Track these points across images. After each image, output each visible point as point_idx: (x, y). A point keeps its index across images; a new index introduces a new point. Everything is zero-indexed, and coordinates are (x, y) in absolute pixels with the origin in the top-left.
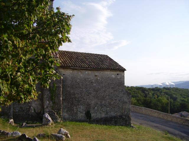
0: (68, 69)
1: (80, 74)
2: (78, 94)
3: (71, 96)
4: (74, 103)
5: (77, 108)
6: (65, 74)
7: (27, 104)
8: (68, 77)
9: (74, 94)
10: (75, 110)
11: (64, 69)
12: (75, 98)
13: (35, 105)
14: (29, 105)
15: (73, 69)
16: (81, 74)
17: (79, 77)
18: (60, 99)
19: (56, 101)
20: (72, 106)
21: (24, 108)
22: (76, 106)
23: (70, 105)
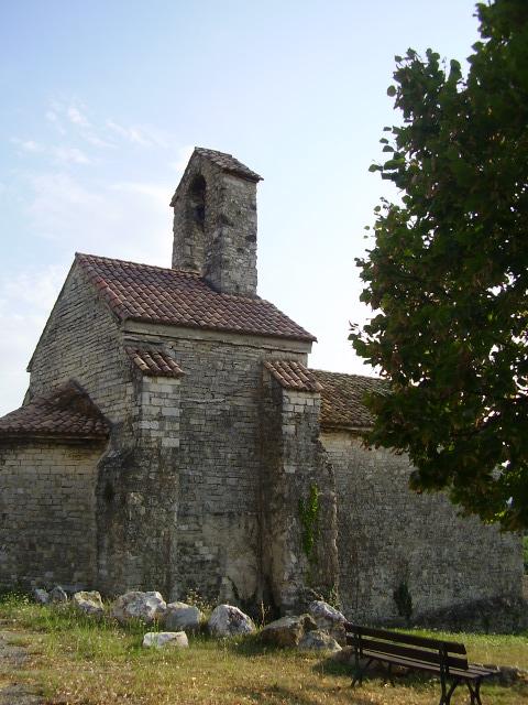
2: (372, 525)
5: (368, 578)
7: (211, 569)
8: (339, 463)
9: (359, 526)
10: (362, 583)
12: (363, 539)
17: (372, 463)
18: (328, 548)
22: (367, 570)
23: (346, 565)
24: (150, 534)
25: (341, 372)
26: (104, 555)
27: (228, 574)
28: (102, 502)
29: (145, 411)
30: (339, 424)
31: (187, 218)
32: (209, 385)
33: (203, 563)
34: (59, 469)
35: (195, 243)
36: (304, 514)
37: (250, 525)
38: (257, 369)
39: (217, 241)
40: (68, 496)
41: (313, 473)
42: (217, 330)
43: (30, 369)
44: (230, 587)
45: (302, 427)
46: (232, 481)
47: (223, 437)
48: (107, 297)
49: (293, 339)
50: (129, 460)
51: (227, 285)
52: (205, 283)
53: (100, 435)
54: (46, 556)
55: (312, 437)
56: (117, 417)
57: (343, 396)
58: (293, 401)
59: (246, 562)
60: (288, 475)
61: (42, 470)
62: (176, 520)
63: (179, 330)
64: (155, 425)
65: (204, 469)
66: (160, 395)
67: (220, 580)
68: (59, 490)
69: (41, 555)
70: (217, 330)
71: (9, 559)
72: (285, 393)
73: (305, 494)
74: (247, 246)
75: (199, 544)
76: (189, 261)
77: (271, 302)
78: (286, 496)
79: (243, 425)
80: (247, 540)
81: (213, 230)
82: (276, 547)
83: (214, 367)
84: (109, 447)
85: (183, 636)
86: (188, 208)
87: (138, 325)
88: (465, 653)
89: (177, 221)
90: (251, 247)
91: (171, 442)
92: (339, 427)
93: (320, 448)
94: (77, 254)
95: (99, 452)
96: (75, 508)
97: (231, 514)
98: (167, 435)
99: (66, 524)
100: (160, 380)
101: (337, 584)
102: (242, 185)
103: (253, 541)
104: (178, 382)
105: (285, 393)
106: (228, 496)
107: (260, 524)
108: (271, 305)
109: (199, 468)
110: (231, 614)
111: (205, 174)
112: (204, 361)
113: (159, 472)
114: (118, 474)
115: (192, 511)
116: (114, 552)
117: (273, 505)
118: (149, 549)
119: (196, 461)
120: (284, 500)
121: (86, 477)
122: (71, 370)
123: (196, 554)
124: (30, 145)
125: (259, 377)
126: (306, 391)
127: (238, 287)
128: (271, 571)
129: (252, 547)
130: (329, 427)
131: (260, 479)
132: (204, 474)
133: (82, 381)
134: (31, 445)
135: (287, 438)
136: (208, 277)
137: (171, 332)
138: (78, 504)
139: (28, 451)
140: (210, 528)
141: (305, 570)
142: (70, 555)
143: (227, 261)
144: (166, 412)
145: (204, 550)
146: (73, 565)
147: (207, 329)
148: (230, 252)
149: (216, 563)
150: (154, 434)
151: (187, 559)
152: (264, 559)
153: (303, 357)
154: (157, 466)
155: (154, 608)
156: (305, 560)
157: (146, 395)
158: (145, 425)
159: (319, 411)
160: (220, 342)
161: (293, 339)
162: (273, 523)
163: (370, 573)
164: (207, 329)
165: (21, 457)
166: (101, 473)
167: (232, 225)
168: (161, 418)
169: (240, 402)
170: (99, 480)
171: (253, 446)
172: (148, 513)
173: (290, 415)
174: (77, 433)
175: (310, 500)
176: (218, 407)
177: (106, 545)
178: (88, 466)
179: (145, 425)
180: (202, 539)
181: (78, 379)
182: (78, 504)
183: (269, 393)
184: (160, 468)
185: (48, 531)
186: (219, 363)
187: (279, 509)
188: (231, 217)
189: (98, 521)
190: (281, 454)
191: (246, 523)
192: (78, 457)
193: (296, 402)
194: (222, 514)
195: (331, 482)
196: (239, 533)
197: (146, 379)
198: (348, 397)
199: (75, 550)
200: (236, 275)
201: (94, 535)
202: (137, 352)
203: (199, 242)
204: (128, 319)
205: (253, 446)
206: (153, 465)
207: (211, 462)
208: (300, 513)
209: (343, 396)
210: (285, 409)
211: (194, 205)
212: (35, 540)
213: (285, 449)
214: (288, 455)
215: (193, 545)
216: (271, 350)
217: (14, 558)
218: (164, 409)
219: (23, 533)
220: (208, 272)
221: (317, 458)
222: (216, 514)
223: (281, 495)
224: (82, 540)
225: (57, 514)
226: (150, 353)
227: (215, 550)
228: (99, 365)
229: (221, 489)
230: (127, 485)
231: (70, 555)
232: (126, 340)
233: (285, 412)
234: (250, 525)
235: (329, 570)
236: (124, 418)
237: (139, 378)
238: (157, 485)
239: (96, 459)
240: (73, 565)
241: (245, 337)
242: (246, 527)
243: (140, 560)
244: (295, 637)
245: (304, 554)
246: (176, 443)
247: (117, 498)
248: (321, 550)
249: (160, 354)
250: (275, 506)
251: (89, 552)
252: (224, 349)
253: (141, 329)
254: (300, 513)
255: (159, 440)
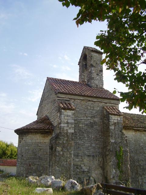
0: (130, 130)
1: (143, 136)
2: (143, 161)
3: (135, 163)
4: (139, 172)
5: (142, 179)
6: (127, 136)
7: (86, 174)
8: (131, 140)
9: (138, 161)
10: (140, 180)
11: (126, 130)
12: (140, 166)
13: (95, 176)
14: (89, 174)
15: (136, 130)
16: (145, 136)
17: (142, 140)
18: (127, 167)
19: (123, 169)
20: (137, 176)
21: (82, 179)
22: (141, 176)
23: (134, 174)
24: (64, 160)
25: (133, 113)
26: (50, 168)
27: (92, 176)
28: (51, 151)
29: (62, 121)
30: (130, 127)
31: (83, 67)
32: (85, 114)
33: (84, 172)
34: (38, 141)
35: (85, 75)
36: (118, 156)
37: (100, 160)
38: (101, 109)
39: (90, 72)
40: (41, 149)
41: (120, 142)
42: (88, 96)
43: (37, 114)
44: (93, 180)
45: (117, 127)
46: (94, 145)
47: (90, 131)
48: (54, 88)
49: (113, 99)
50: (57, 137)
51: (93, 85)
52: (87, 85)
53: (50, 130)
54: (34, 168)
55: (120, 130)
56: (55, 124)
57: (133, 119)
58: (113, 118)
59: (99, 172)
60: (112, 143)
61: (34, 141)
62: (73, 156)
63: (75, 96)
64: (66, 125)
65: (84, 141)
66: (67, 116)
67: (90, 178)
68: (38, 147)
69: (32, 168)
70: (88, 96)
71: (23, 169)
72: (110, 116)
73: (118, 149)
74: (100, 73)
75: (82, 165)
76: (83, 80)
77: (104, 84)
78: (111, 150)
79: (97, 127)
80: (99, 165)
81: (89, 69)
82: (108, 167)
83: (87, 108)
84: (53, 134)
85: (51, 190)
86: (83, 65)
87: (62, 95)
88: (109, 183)
89: (80, 69)
90: (101, 73)
91: (71, 131)
92: (130, 128)
93: (123, 134)
94: (47, 78)
95: (51, 135)
96: (43, 153)
97: (93, 156)
98: (70, 129)
99: (40, 158)
100: (67, 111)
101: (130, 180)
102: (98, 55)
103: (101, 165)
104: (73, 112)
105: (110, 116)
106: (92, 150)
107: (103, 159)
108: (108, 91)
109: (82, 140)
110: (72, 183)
111: (87, 53)
112: (84, 106)
113: (67, 140)
114: (54, 141)
115: (80, 154)
116: (53, 167)
117: (107, 153)
118: (63, 166)
119: (81, 138)
120: (111, 151)
121: (46, 143)
122: (45, 113)
123: (82, 169)
124: (55, 66)
125: (102, 112)
126: (117, 115)
127: (97, 86)
128: (107, 175)
129: (101, 167)
130: (126, 128)
131: (103, 145)
132: (84, 143)
133: (48, 115)
134: (30, 134)
135: (111, 130)
136: (88, 83)
137: (73, 97)
138: (44, 152)
139: (30, 135)
140: (86, 160)
141: (118, 175)
142: (41, 168)
143: (93, 78)
144: (69, 121)
145: (84, 168)
146: (42, 171)
147: (84, 96)
148: (94, 75)
149: (88, 172)
150: (65, 128)
151: (78, 170)
152: (105, 171)
153: (116, 105)
154: (66, 138)
155: (50, 181)
156: (118, 171)
157: (63, 116)
158: (62, 125)
159: (122, 122)
160: (89, 100)
161: (113, 99)
162: (107, 159)
163: (143, 177)
164: (84, 96)
165: (27, 137)
166: (50, 142)
167: (95, 67)
168: (68, 123)
169: (96, 120)
170: (50, 144)
171: (101, 134)
172: (63, 154)
173: (112, 123)
174: (43, 129)
175: (120, 151)
176: (89, 121)
177: (51, 165)
178: (47, 140)
179: (62, 125)
180: (83, 164)
181: (47, 114)
182: (44, 152)
183: (105, 116)
184: (67, 139)
185: (35, 161)
186: (89, 107)
187: (109, 154)
188: (94, 64)
189: (49, 157)
190: (109, 136)
191: (99, 159)
192: (44, 137)
193: (114, 119)
194: (90, 156)
195: (127, 145)
196: (96, 162)
197: (63, 111)
198: (135, 120)
199: (43, 167)
200: (97, 82)
201: (48, 162)
202: (61, 103)
203: (86, 74)
204: (58, 93)
205: (101, 134)
206: (65, 138)
207: (86, 139)
208: (116, 155)
209: (133, 119)
210: (110, 121)
211: (84, 63)
212: (30, 163)
213: (111, 134)
214: (112, 136)
215: (80, 166)
216: (106, 103)
217: (25, 169)
218: (69, 120)
219: (28, 161)
220: (88, 82)
221: (122, 137)
222: (88, 156)
223: (110, 149)
224: (45, 163)
225: (37, 155)
226: (65, 103)
227: (88, 168)
228: (52, 109)
229: (90, 148)
230: (56, 145)
231: (41, 168)
232: (58, 99)
233: (110, 122)
234: (100, 160)
235: (127, 175)
236: (57, 124)
237: (61, 110)
238: (66, 145)
239: (50, 138)
240: (42, 171)
241: (97, 99)
242: (99, 160)
243: (60, 169)
244: (91, 191)
245: (118, 170)
246: (73, 131)
247: (54, 149)
248: (124, 168)
249: (69, 103)
250: (108, 153)
251: (47, 167)
252: (90, 103)
253: (63, 96)
254: (116, 155)
255: (67, 130)
